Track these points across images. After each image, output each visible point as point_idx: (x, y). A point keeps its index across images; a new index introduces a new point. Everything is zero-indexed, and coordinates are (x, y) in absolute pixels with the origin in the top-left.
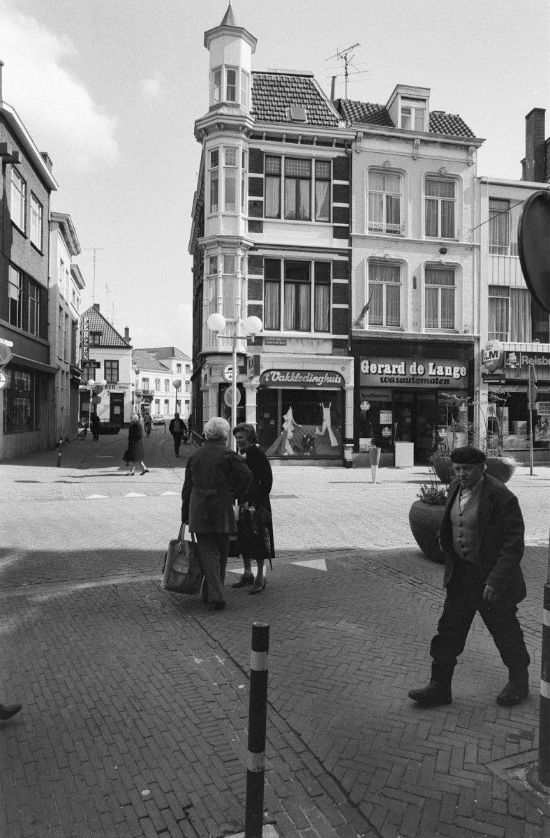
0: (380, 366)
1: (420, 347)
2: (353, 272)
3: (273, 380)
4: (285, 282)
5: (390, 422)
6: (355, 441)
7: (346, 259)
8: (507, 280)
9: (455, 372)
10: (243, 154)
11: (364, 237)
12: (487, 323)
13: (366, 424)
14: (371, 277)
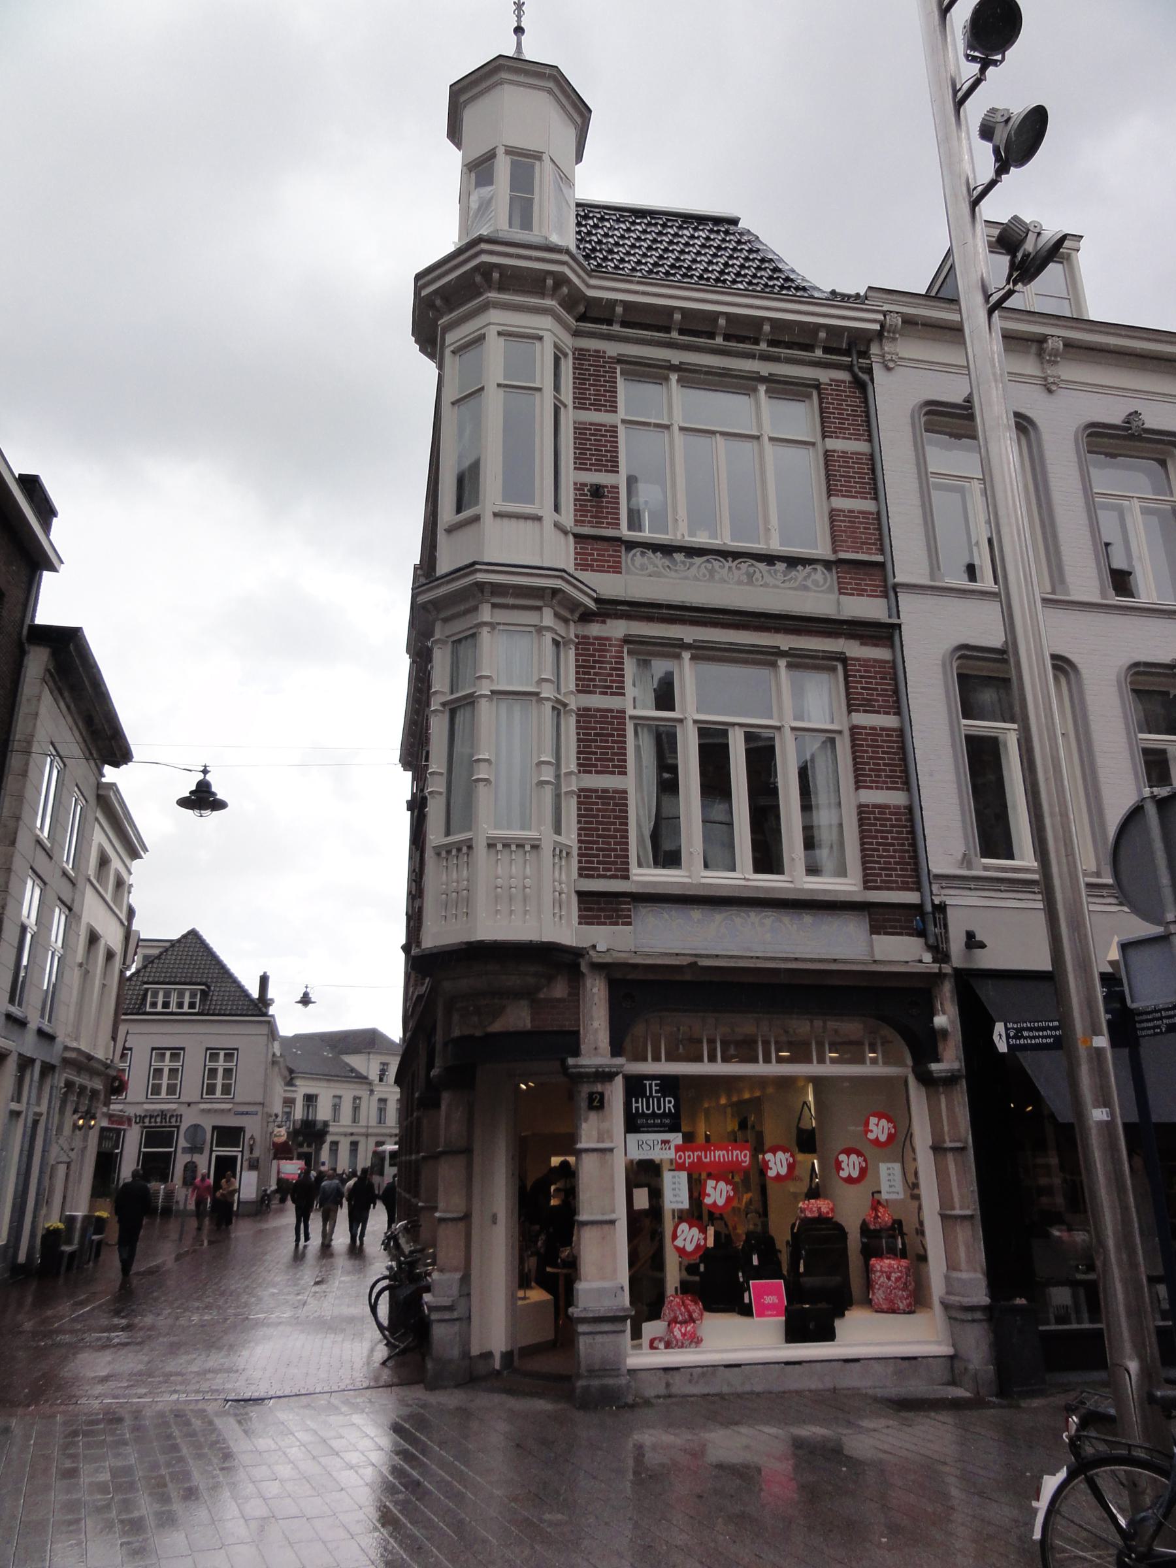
7: (880, 653)
10: (557, 361)
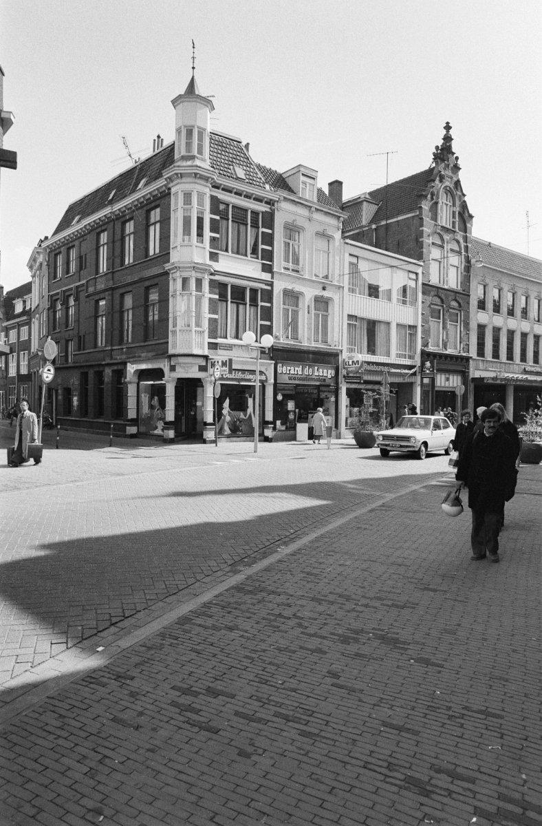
0: (289, 368)
1: (311, 355)
2: (274, 298)
3: (224, 376)
4: (250, 305)
5: (294, 409)
6: (274, 423)
7: (269, 288)
8: (356, 312)
9: (329, 373)
11: (281, 274)
12: (486, 349)
13: (280, 409)
14: (284, 304)
